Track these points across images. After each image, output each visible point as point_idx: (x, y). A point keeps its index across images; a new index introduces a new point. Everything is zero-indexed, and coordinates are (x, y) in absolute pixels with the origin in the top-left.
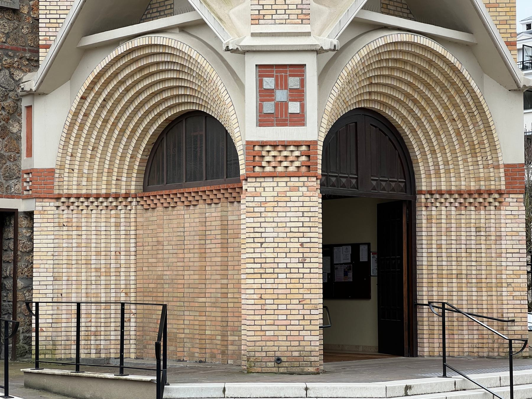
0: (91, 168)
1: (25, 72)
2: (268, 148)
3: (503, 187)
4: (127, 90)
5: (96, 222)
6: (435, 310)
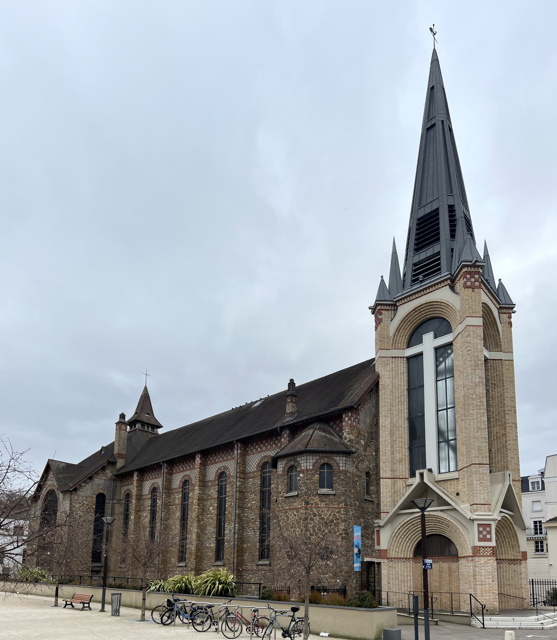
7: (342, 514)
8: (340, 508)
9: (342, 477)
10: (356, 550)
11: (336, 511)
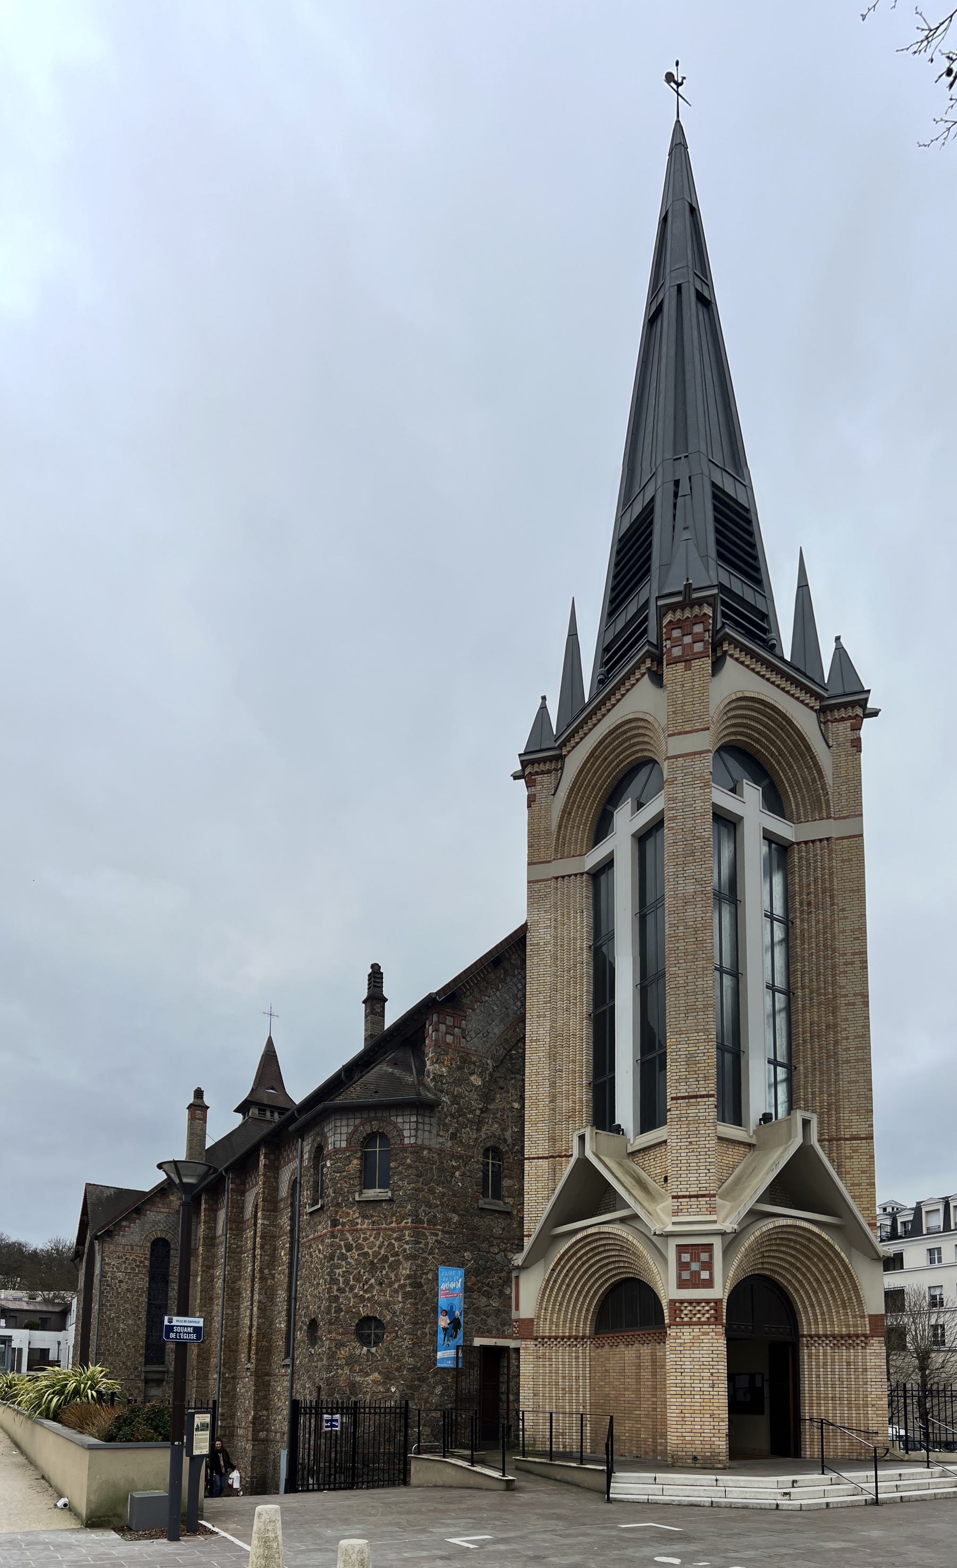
0: (558, 1318)
1: (515, 1254)
2: (686, 1304)
3: (868, 1332)
4: (583, 1264)
5: (562, 1356)
6: (815, 1424)
7: (407, 1243)
8: (402, 1230)
9: (408, 1161)
10: (443, 1321)
11: (395, 1235)
